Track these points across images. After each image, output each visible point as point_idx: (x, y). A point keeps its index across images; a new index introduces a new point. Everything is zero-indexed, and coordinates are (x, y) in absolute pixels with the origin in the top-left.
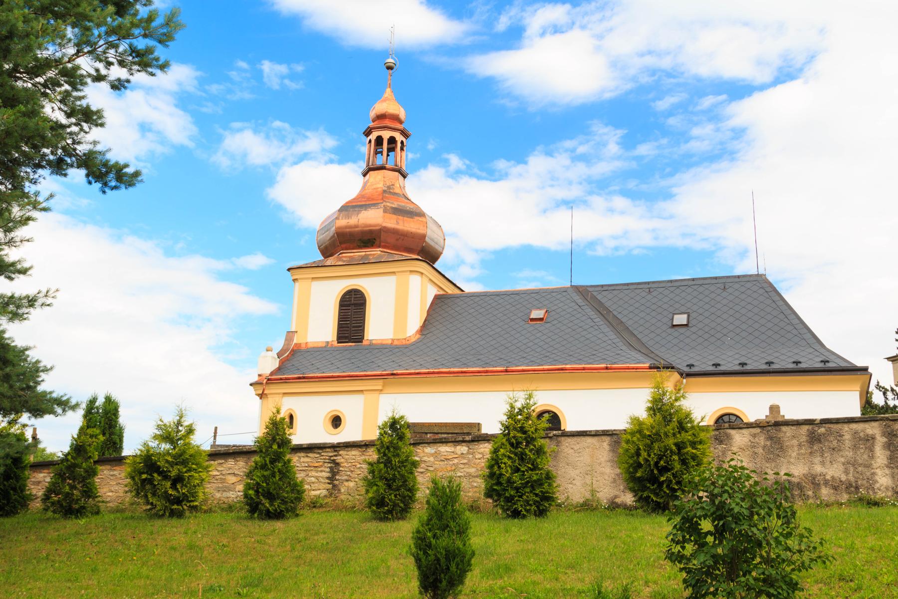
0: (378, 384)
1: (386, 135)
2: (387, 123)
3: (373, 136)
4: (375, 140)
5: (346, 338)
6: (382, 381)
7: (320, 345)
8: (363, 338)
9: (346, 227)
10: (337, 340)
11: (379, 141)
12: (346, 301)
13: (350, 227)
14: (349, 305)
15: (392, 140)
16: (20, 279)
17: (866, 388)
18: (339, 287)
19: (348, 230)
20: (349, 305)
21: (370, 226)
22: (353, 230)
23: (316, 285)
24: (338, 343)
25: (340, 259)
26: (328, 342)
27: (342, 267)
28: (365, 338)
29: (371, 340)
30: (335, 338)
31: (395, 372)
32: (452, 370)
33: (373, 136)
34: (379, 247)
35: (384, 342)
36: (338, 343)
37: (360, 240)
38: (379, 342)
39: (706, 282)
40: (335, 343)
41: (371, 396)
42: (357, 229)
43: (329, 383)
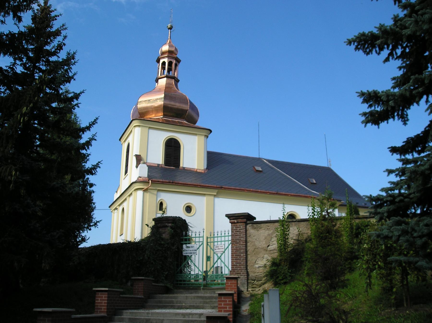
19: (170, 106)
30: (163, 163)
38: (189, 169)
42: (175, 107)
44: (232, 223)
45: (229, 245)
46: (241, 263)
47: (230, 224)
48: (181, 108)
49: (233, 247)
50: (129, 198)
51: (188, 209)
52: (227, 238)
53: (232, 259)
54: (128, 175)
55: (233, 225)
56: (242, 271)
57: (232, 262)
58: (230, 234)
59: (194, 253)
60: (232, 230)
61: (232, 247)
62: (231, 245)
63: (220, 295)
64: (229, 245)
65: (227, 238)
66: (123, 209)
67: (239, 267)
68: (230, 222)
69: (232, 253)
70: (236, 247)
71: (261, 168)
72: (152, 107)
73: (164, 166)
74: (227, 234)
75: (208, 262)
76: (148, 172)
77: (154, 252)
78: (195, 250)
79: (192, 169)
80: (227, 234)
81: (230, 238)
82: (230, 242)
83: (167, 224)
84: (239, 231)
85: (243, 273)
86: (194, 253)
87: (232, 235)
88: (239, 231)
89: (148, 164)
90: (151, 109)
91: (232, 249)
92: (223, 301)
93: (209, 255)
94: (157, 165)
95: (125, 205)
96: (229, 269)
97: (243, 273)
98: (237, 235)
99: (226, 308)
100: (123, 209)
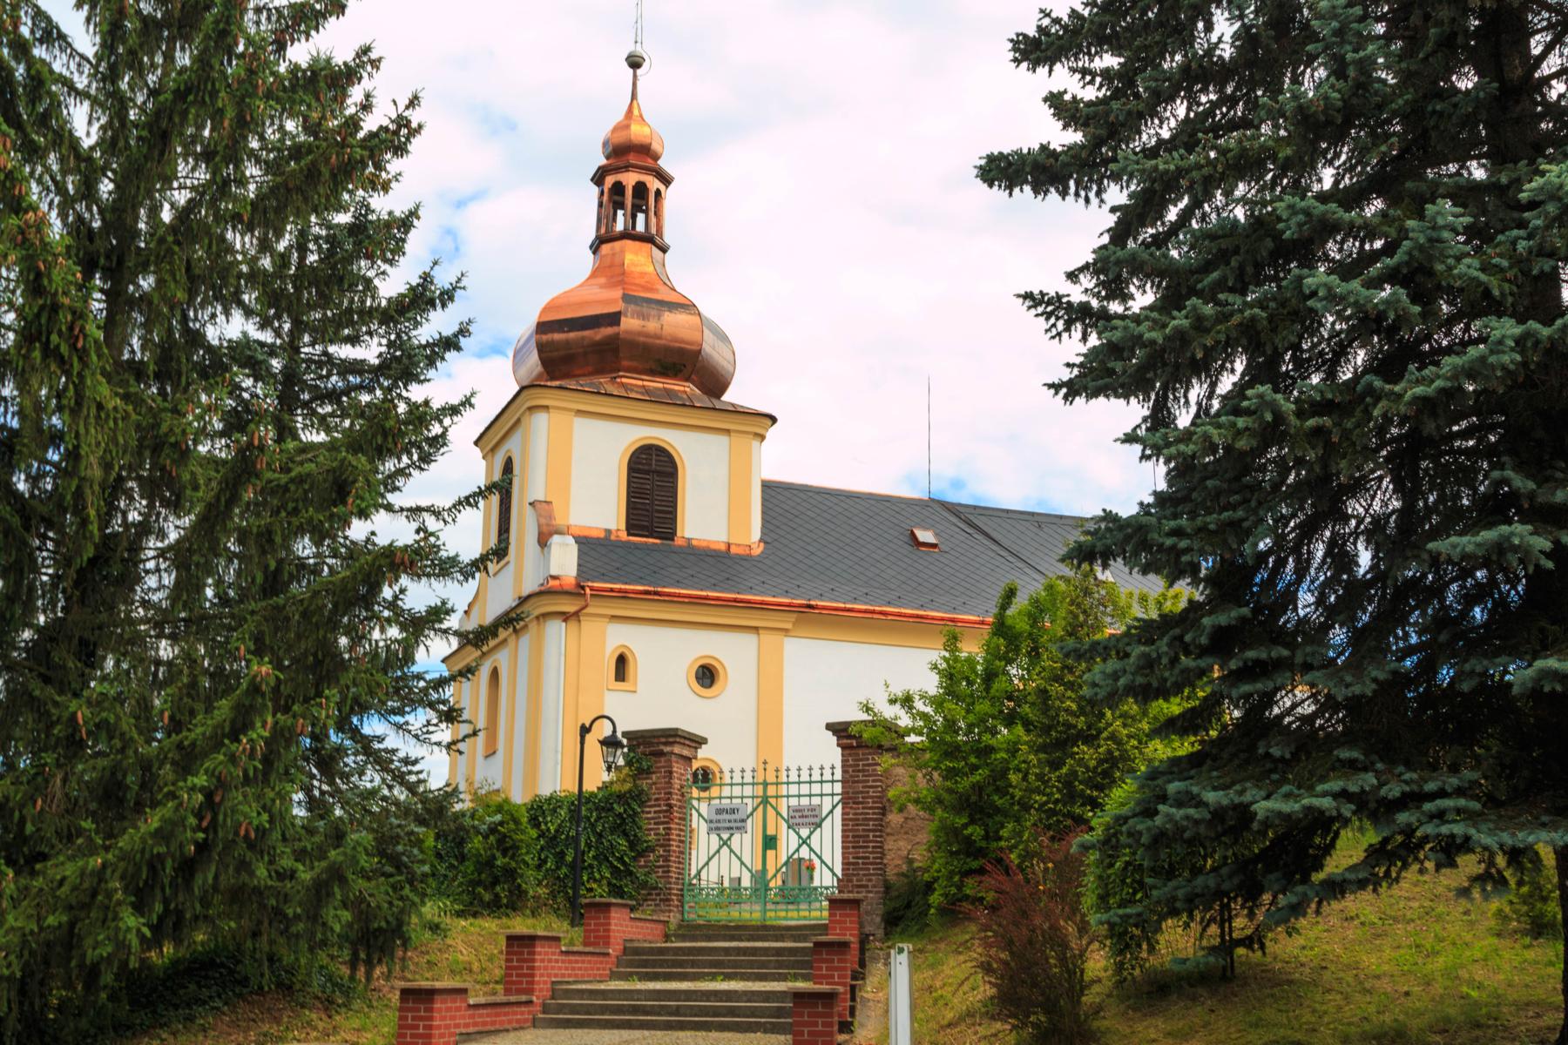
0: (786, 621)
1: (630, 179)
2: (633, 159)
3: (610, 180)
4: (634, 187)
5: (643, 528)
6: (795, 615)
7: (595, 534)
8: (674, 533)
9: (640, 334)
10: (628, 529)
11: (618, 188)
12: (640, 463)
13: (647, 335)
14: (647, 472)
15: (641, 190)
16: (223, 317)
17: (458, 656)
18: (632, 436)
19: (642, 339)
20: (647, 472)
21: (683, 341)
22: (650, 340)
23: (582, 427)
24: (629, 534)
25: (591, 385)
26: (608, 532)
27: (639, 404)
28: (679, 533)
29: (689, 539)
30: (623, 526)
31: (813, 603)
32: (903, 611)
33: (610, 180)
34: (687, 380)
35: (713, 546)
36: (629, 534)
37: (659, 360)
38: (704, 544)
39: (995, 513)
40: (624, 536)
41: (767, 638)
42: (658, 342)
43: (754, 612)
44: (844, 747)
45: (834, 807)
46: (868, 858)
47: (839, 750)
48: (677, 345)
49: (848, 814)
50: (518, 639)
51: (707, 675)
52: (827, 788)
53: (843, 848)
54: (508, 563)
55: (847, 752)
56: (870, 880)
57: (843, 853)
58: (838, 775)
59: (737, 828)
60: (843, 766)
61: (843, 814)
62: (840, 806)
63: (817, 944)
64: (834, 807)
65: (827, 788)
66: (495, 673)
67: (862, 869)
68: (838, 745)
69: (843, 831)
70: (855, 814)
71: (936, 535)
72: (585, 343)
73: (624, 536)
74: (827, 776)
75: (770, 853)
76: (579, 558)
77: (53, 711)
78: (743, 821)
79: (714, 542)
80: (827, 776)
81: (838, 788)
82: (837, 798)
83: (662, 747)
84: (863, 771)
85: (874, 886)
86: (737, 828)
87: (844, 781)
88: (863, 771)
89: (578, 532)
90: (581, 350)
91: (843, 820)
92: (826, 961)
93: (771, 832)
94: (602, 535)
95: (502, 658)
96: (834, 874)
97: (874, 886)
98: (858, 782)
99: (816, 1024)
100: (495, 673)
